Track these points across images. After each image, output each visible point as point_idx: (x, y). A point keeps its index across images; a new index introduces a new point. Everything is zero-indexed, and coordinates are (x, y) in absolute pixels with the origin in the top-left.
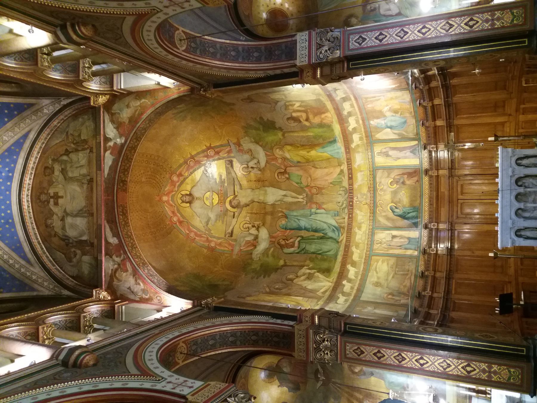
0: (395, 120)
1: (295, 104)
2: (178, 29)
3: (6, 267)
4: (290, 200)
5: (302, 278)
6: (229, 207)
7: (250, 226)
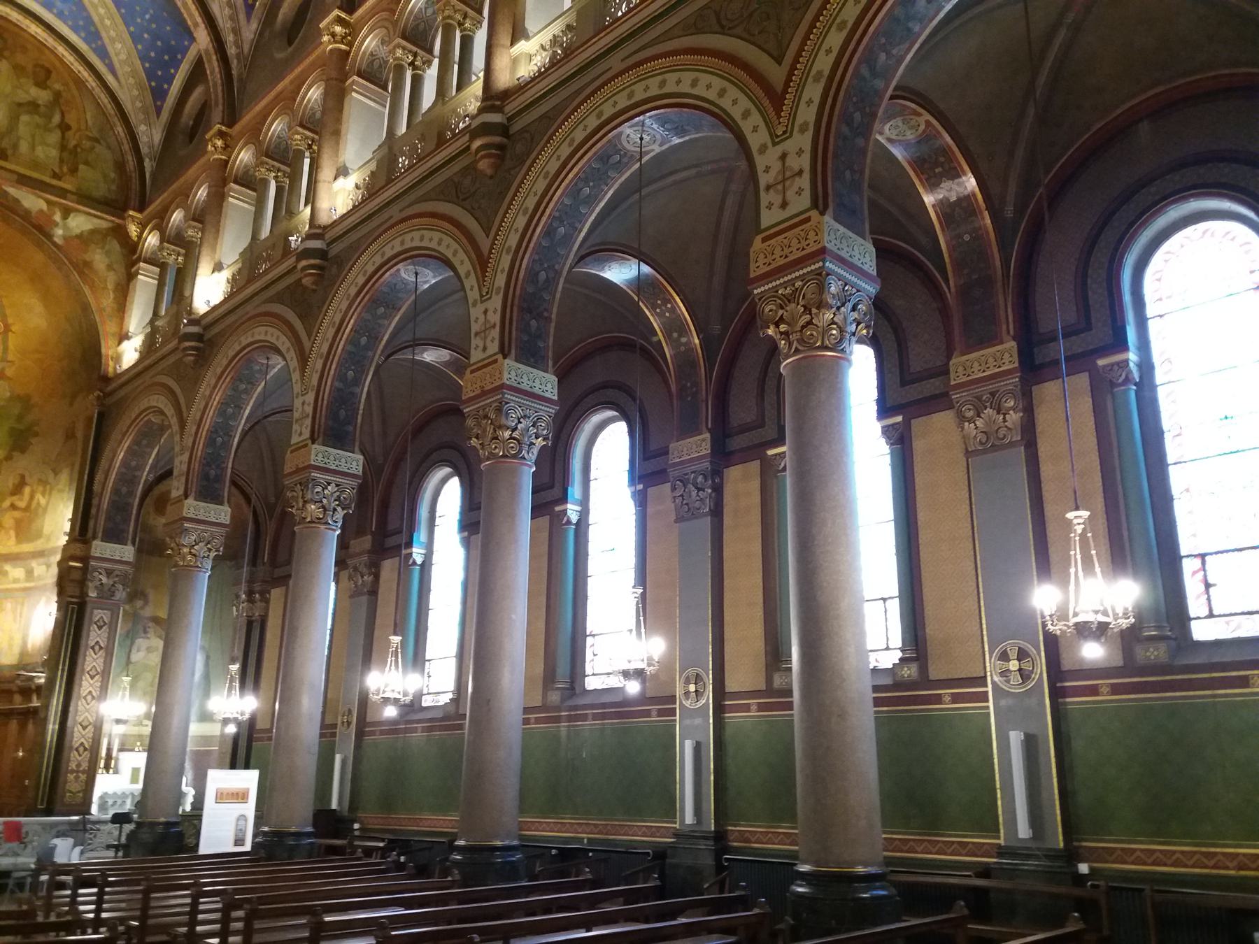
1: (44, 496)
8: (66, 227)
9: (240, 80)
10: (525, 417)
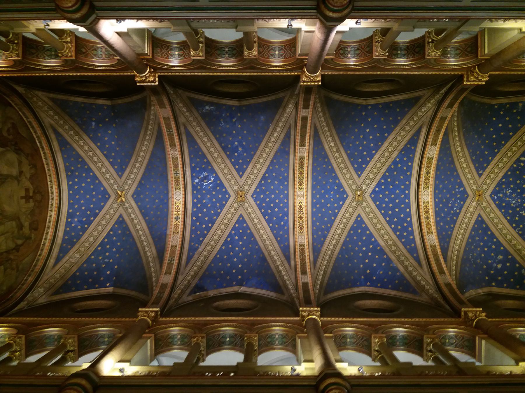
3: (77, 128)
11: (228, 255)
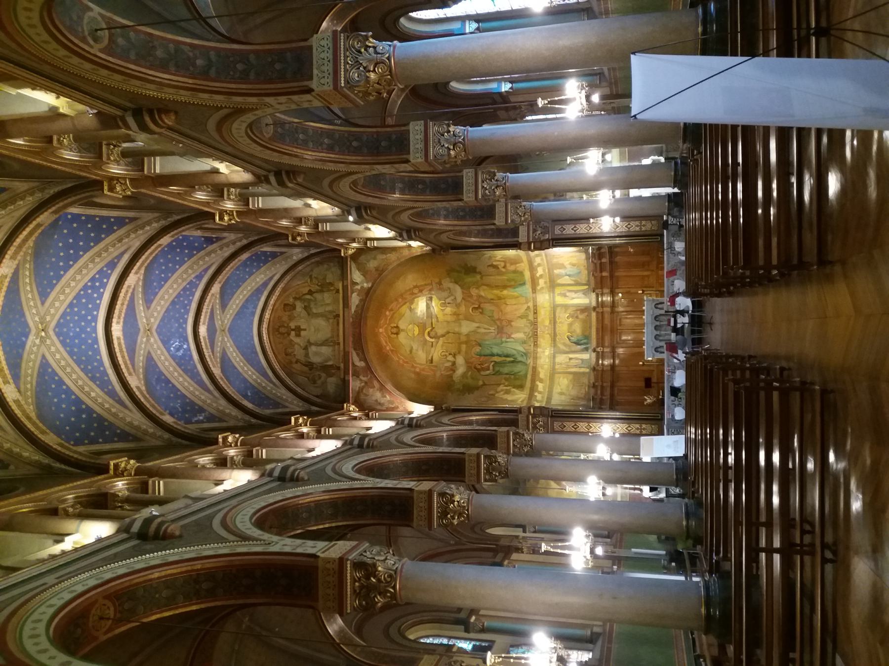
0: (570, 270)
2: (90, 9)
3: (260, 389)
4: (483, 331)
5: (502, 393)
6: (428, 338)
7: (447, 354)
8: (362, 282)
9: (259, 234)
10: (439, 142)
11: (167, 267)
